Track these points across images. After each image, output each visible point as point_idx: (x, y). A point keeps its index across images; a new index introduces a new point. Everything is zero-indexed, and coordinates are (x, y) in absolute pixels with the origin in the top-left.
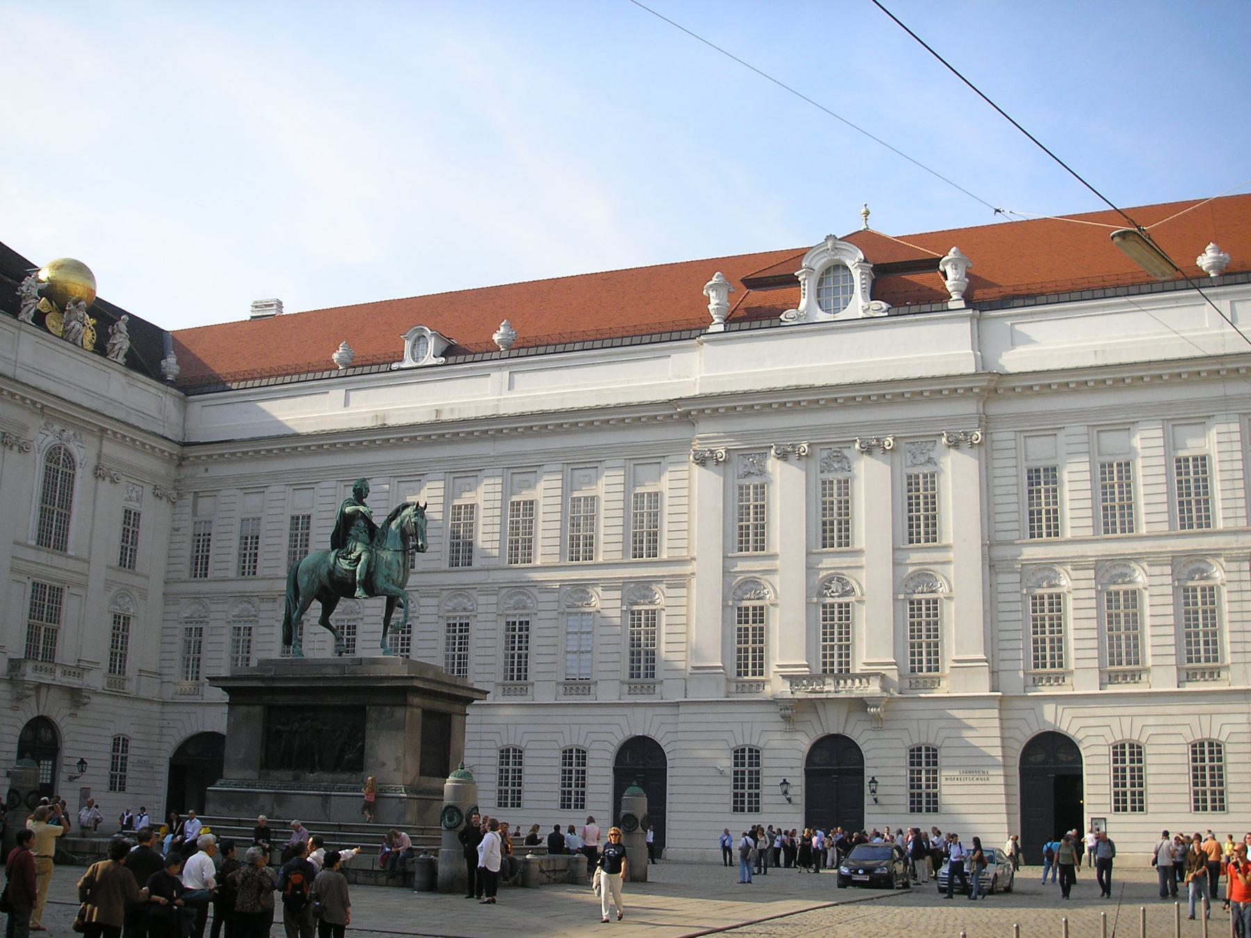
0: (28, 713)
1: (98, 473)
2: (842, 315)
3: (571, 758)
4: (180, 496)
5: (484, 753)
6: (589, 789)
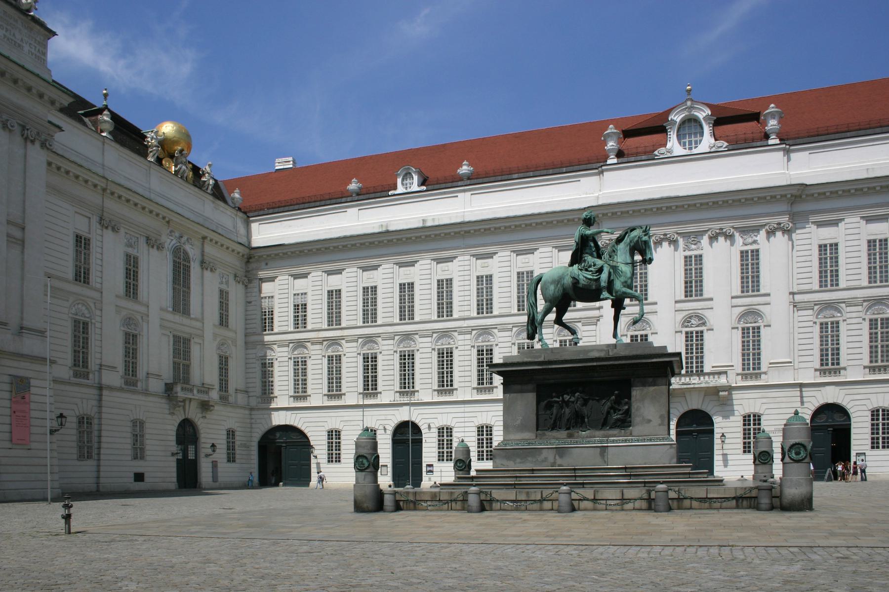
2: (695, 151)
4: (250, 281)
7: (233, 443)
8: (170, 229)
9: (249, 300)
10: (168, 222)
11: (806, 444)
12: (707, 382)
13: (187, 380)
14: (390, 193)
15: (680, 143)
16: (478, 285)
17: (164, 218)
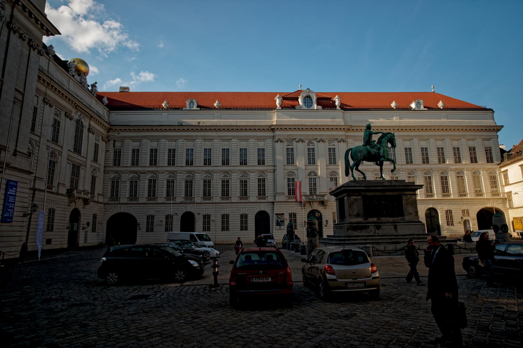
0: (73, 206)
1: (89, 130)
4: (109, 141)
6: (249, 225)
9: (107, 150)
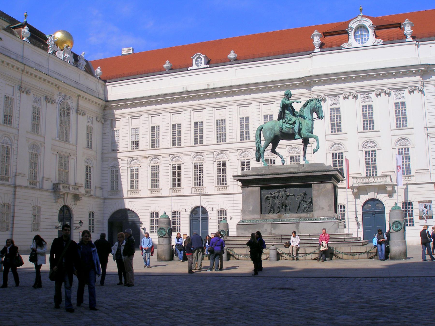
3: (175, 214)
4: (105, 121)
5: (235, 211)
7: (93, 220)
8: (59, 91)
10: (58, 88)
11: (401, 222)
12: (379, 182)
13: (66, 182)
14: (188, 69)
15: (356, 40)
16: (241, 123)
17: (56, 85)
